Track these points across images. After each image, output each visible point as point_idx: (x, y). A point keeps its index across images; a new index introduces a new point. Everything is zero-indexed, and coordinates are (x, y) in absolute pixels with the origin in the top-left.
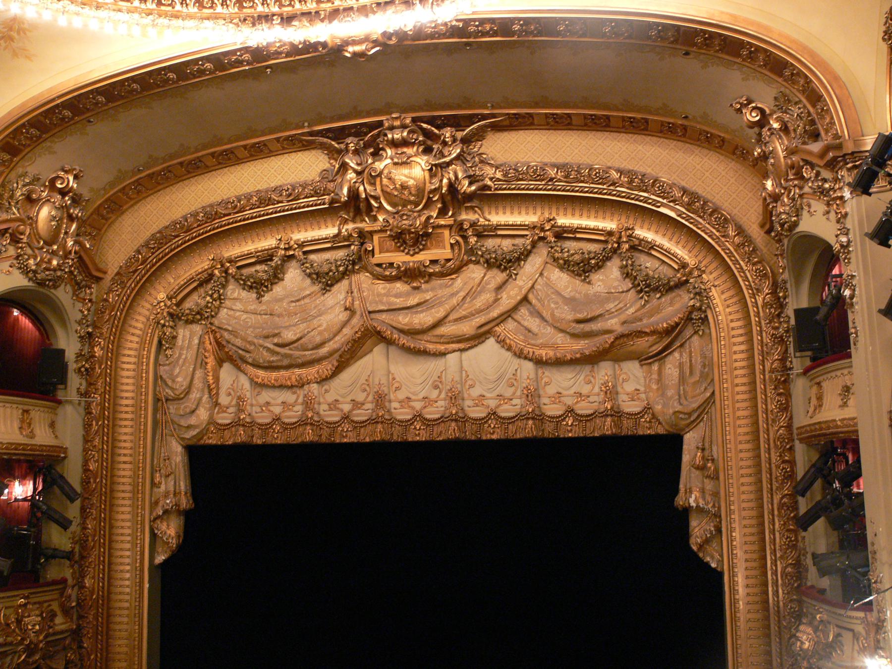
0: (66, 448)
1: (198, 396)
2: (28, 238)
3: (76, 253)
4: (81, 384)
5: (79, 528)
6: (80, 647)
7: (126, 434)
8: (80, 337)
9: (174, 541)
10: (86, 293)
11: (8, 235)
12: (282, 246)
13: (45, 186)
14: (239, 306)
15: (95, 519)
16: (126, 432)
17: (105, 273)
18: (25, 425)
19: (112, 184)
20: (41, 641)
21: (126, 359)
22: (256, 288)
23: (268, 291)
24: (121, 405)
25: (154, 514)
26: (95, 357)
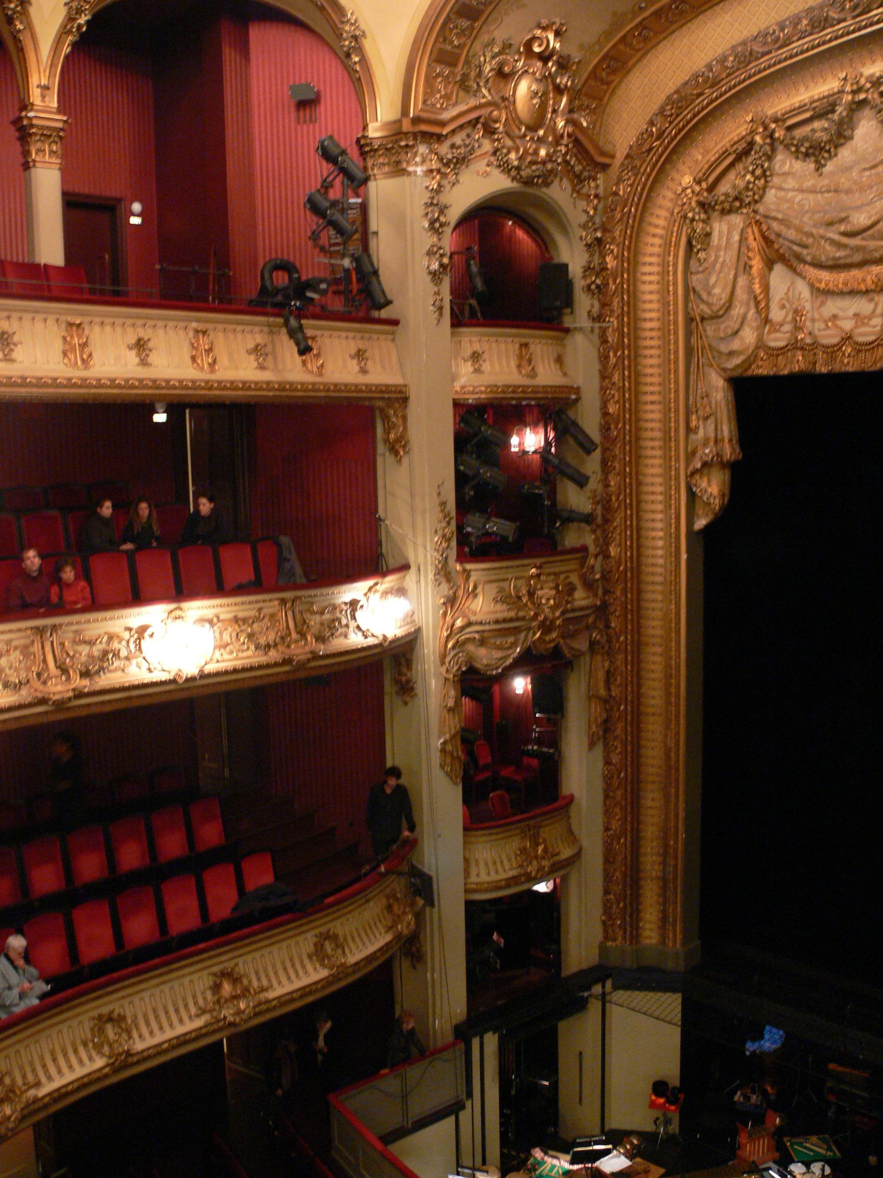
0: (578, 388)
1: (742, 311)
2: (505, 125)
3: (569, 135)
4: (592, 306)
5: (600, 487)
6: (608, 627)
7: (651, 366)
8: (587, 245)
9: (717, 501)
10: (590, 188)
11: (479, 126)
12: (848, 88)
13: (521, 53)
14: (791, 183)
15: (618, 474)
16: (651, 363)
17: (612, 157)
18: (524, 363)
19: (608, 35)
20: (558, 618)
21: (646, 269)
22: (814, 154)
23: (830, 158)
24: (644, 330)
25: (691, 468)
26: (607, 269)
